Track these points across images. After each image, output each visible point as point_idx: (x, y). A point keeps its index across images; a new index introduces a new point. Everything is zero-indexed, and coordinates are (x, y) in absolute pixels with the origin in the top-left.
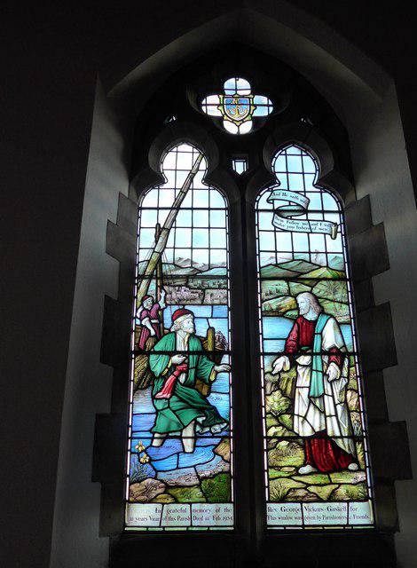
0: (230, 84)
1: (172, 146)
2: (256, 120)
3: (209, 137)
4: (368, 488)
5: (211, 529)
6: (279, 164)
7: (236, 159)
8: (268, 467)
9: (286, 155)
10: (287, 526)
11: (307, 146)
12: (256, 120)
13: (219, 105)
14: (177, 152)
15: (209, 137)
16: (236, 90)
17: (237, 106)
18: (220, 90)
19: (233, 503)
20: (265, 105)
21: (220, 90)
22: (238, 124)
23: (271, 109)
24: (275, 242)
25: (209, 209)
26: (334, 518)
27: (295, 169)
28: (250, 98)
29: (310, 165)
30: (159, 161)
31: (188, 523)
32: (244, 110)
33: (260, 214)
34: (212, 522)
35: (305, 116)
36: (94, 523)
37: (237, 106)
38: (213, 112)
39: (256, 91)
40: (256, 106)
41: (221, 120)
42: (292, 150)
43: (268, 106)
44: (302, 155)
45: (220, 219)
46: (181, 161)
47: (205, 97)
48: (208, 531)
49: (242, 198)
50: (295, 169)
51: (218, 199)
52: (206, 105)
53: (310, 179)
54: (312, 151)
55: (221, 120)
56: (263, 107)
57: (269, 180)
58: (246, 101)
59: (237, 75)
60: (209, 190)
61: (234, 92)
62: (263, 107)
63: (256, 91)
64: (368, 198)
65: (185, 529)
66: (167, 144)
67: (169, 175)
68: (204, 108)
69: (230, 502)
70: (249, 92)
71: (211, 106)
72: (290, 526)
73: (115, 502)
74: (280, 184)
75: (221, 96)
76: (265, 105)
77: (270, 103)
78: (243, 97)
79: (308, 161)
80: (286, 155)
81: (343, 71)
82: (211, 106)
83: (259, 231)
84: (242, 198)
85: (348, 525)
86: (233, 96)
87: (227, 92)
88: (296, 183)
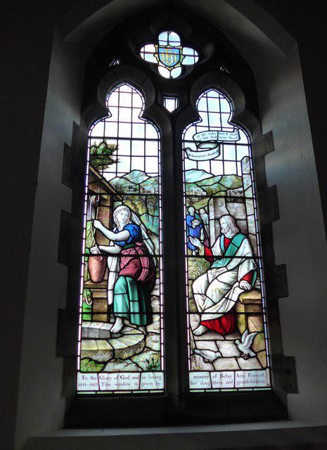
0: (163, 37)
1: (115, 86)
2: (184, 68)
3: (146, 79)
4: (161, 356)
5: (222, 390)
6: (201, 104)
7: (170, 97)
8: (82, 339)
9: (207, 97)
10: (115, 391)
11: (226, 92)
12: (184, 68)
13: (154, 54)
14: (119, 92)
15: (146, 79)
16: (168, 42)
17: (169, 54)
18: (155, 41)
19: (163, 371)
20: (191, 56)
21: (155, 41)
22: (170, 69)
23: (197, 59)
24: (199, 169)
25: (131, 139)
26: (124, 384)
27: (214, 108)
28: (180, 49)
29: (226, 106)
30: (105, 100)
31: (97, 389)
32: (173, 59)
33: (157, 138)
34: (115, 388)
35: (227, 66)
36: (58, 389)
37: (169, 54)
38: (150, 59)
39: (185, 43)
40: (185, 56)
41: (156, 66)
42: (212, 93)
43: (194, 56)
44: (219, 98)
45: (153, 148)
46: (125, 102)
47: (144, 46)
48: (205, 392)
49: (172, 135)
50: (214, 108)
51: (152, 132)
52: (144, 53)
53: (226, 117)
54: (228, 95)
55: (156, 66)
56: (190, 57)
57: (194, 117)
58: (176, 51)
59: (169, 29)
60: (145, 124)
61: (166, 44)
62: (190, 57)
63: (185, 43)
64: (271, 133)
65: (203, 391)
66: (111, 85)
67: (113, 111)
68: (142, 55)
69: (161, 371)
70: (179, 44)
71: (148, 53)
72: (256, 388)
73: (70, 373)
74: (202, 121)
75: (157, 46)
76: (191, 56)
77: (196, 54)
78: (174, 48)
79: (225, 103)
80: (207, 97)
81: (251, 29)
82: (148, 53)
83: (158, 156)
84: (172, 135)
85: (234, 388)
86: (166, 47)
87: (161, 43)
88: (215, 122)
